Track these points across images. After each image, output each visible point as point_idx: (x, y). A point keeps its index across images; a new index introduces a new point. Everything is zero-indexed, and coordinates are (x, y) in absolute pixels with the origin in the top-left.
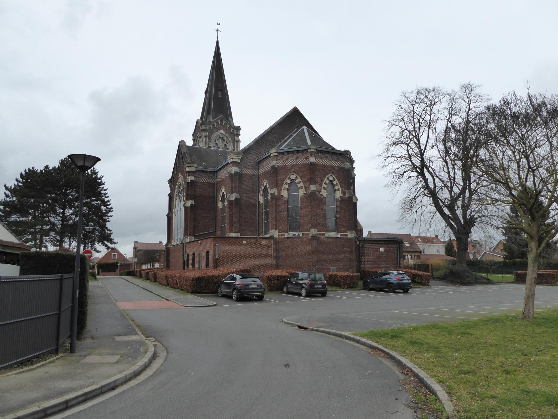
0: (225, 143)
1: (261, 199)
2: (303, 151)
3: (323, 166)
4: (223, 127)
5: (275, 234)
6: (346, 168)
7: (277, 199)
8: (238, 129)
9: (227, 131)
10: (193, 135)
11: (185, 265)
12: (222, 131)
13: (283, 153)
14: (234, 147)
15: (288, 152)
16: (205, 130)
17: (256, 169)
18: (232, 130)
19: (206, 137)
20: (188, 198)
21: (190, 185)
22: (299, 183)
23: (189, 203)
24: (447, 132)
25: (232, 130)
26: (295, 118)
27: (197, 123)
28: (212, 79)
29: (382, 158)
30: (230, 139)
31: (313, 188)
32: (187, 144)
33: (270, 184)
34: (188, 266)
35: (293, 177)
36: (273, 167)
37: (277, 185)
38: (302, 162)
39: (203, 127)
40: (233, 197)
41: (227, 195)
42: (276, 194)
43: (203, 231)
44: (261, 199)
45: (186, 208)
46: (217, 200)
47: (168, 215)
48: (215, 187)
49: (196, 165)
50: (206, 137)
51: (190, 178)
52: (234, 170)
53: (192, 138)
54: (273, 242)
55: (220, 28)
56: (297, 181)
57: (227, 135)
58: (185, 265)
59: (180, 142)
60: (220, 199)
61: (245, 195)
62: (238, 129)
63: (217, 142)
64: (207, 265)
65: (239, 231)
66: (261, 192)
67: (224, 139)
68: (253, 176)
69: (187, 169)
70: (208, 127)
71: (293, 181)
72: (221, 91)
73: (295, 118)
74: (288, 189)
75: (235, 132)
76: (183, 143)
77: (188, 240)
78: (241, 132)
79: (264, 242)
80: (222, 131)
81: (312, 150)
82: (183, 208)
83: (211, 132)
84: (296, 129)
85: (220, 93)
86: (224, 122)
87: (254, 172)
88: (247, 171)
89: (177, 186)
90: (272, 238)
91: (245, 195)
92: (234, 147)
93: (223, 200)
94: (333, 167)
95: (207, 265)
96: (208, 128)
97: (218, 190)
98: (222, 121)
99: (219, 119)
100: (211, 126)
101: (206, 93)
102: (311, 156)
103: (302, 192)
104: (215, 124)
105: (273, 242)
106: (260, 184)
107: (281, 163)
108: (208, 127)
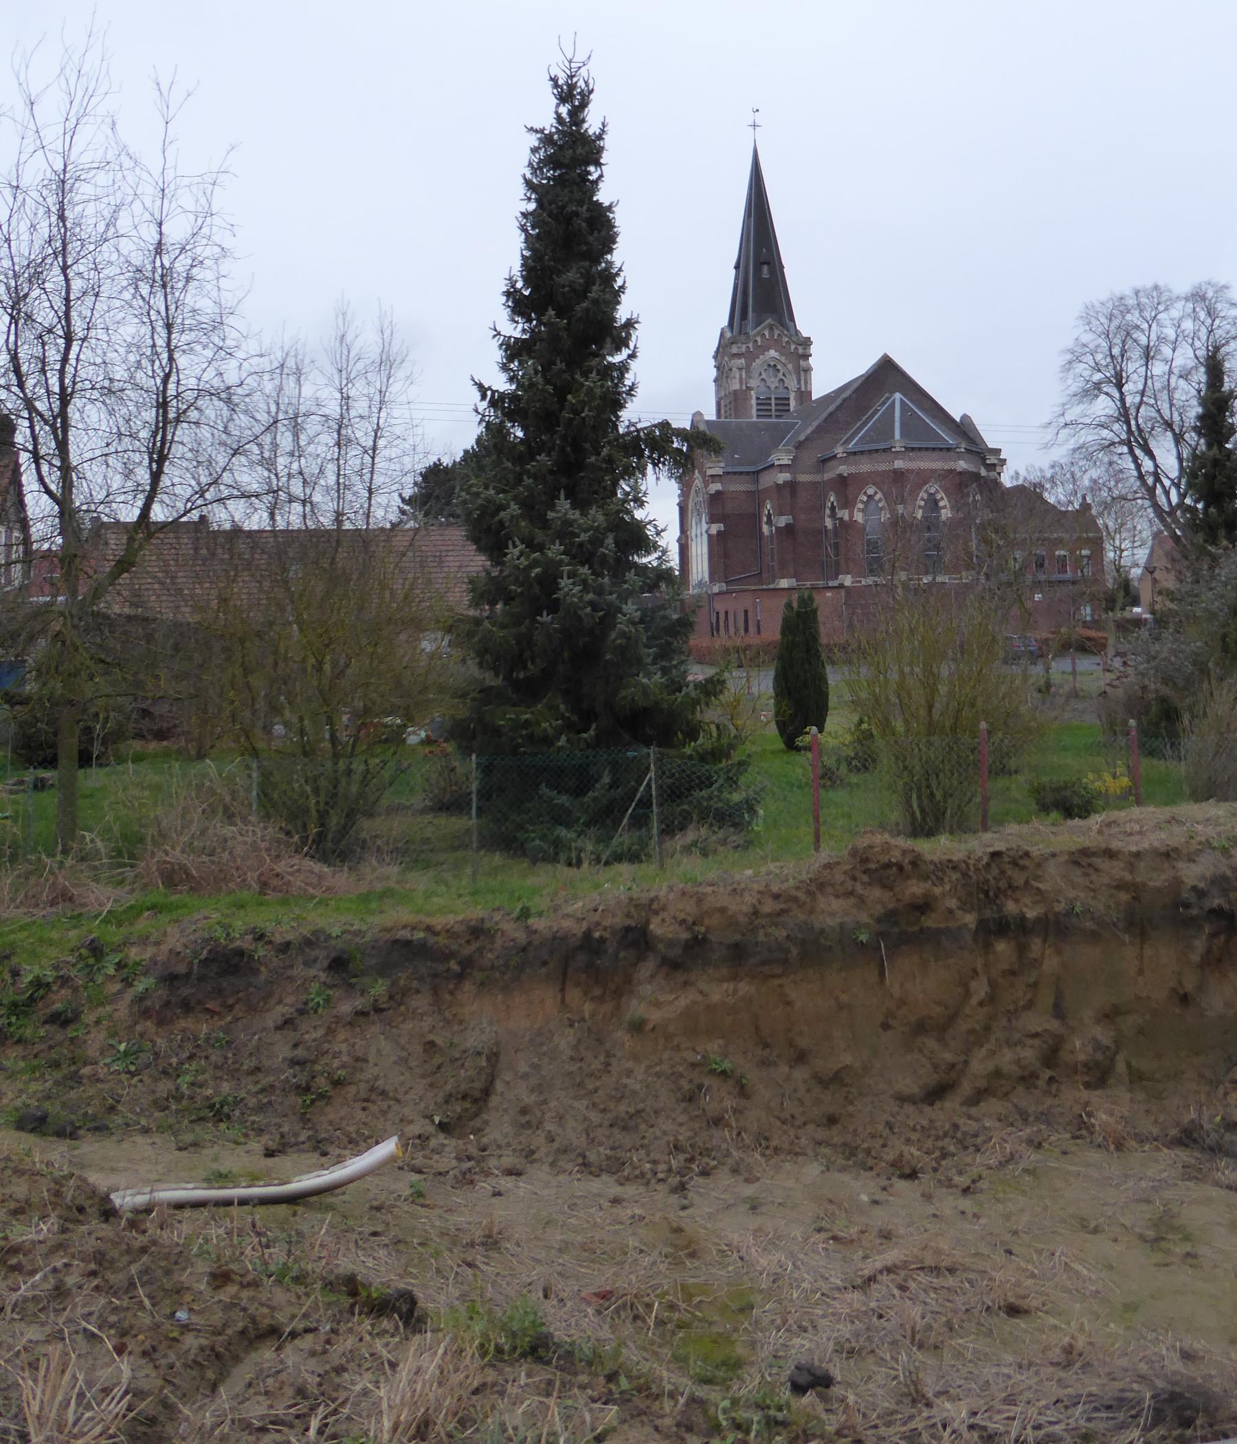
0: (780, 375)
1: (829, 523)
2: (884, 450)
3: (919, 472)
4: (776, 344)
5: (848, 580)
6: (959, 469)
7: (845, 527)
8: (807, 342)
9: (782, 349)
10: (715, 357)
11: (550, 1383)
12: (772, 353)
13: (855, 453)
14: (799, 383)
15: (862, 452)
16: (738, 356)
17: (819, 472)
18: (793, 347)
19: (740, 369)
20: (712, 520)
21: (716, 498)
22: (880, 500)
23: (715, 529)
24: (36, 1080)
25: (793, 347)
26: (886, 375)
27: (722, 335)
28: (748, 240)
29: (1052, 430)
30: (790, 366)
31: (900, 509)
32: (706, 418)
33: (838, 501)
34: (718, 631)
35: (870, 491)
36: (840, 476)
37: (848, 503)
38: (883, 467)
39: (734, 350)
40: (782, 521)
41: (774, 520)
42: (846, 518)
43: (740, 573)
44: (829, 523)
45: (710, 536)
46: (760, 522)
47: (679, 540)
48: (756, 497)
49: (723, 465)
50: (740, 369)
51: (715, 487)
52: (783, 477)
53: (713, 362)
54: (843, 592)
55: (759, 118)
56: (877, 497)
57: (783, 359)
58: (714, 630)
59: (694, 415)
60: (765, 519)
61: (803, 517)
62: (807, 342)
63: (764, 376)
64: (746, 630)
65: (795, 575)
66: (828, 512)
67: (779, 367)
68: (814, 484)
69: (709, 472)
70: (744, 346)
71: (870, 497)
72: (768, 263)
73: (886, 375)
74: (863, 511)
75: (801, 351)
76: (698, 418)
77: (716, 589)
78: (813, 349)
79: (829, 594)
80: (772, 353)
81: (898, 449)
82: (705, 537)
83: (750, 357)
84: (886, 395)
85: (765, 269)
86: (777, 332)
87: (817, 478)
88: (804, 478)
89: (693, 491)
90: (841, 586)
91: (803, 517)
92: (799, 383)
93: (769, 522)
94: (933, 471)
95: (746, 630)
96: (744, 349)
97: (761, 506)
98: (771, 328)
99: (764, 328)
100: (751, 345)
101: (737, 267)
102: (896, 459)
103: (885, 516)
104: (759, 339)
105: (843, 592)
106: (826, 497)
107: (853, 470)
108: (744, 346)
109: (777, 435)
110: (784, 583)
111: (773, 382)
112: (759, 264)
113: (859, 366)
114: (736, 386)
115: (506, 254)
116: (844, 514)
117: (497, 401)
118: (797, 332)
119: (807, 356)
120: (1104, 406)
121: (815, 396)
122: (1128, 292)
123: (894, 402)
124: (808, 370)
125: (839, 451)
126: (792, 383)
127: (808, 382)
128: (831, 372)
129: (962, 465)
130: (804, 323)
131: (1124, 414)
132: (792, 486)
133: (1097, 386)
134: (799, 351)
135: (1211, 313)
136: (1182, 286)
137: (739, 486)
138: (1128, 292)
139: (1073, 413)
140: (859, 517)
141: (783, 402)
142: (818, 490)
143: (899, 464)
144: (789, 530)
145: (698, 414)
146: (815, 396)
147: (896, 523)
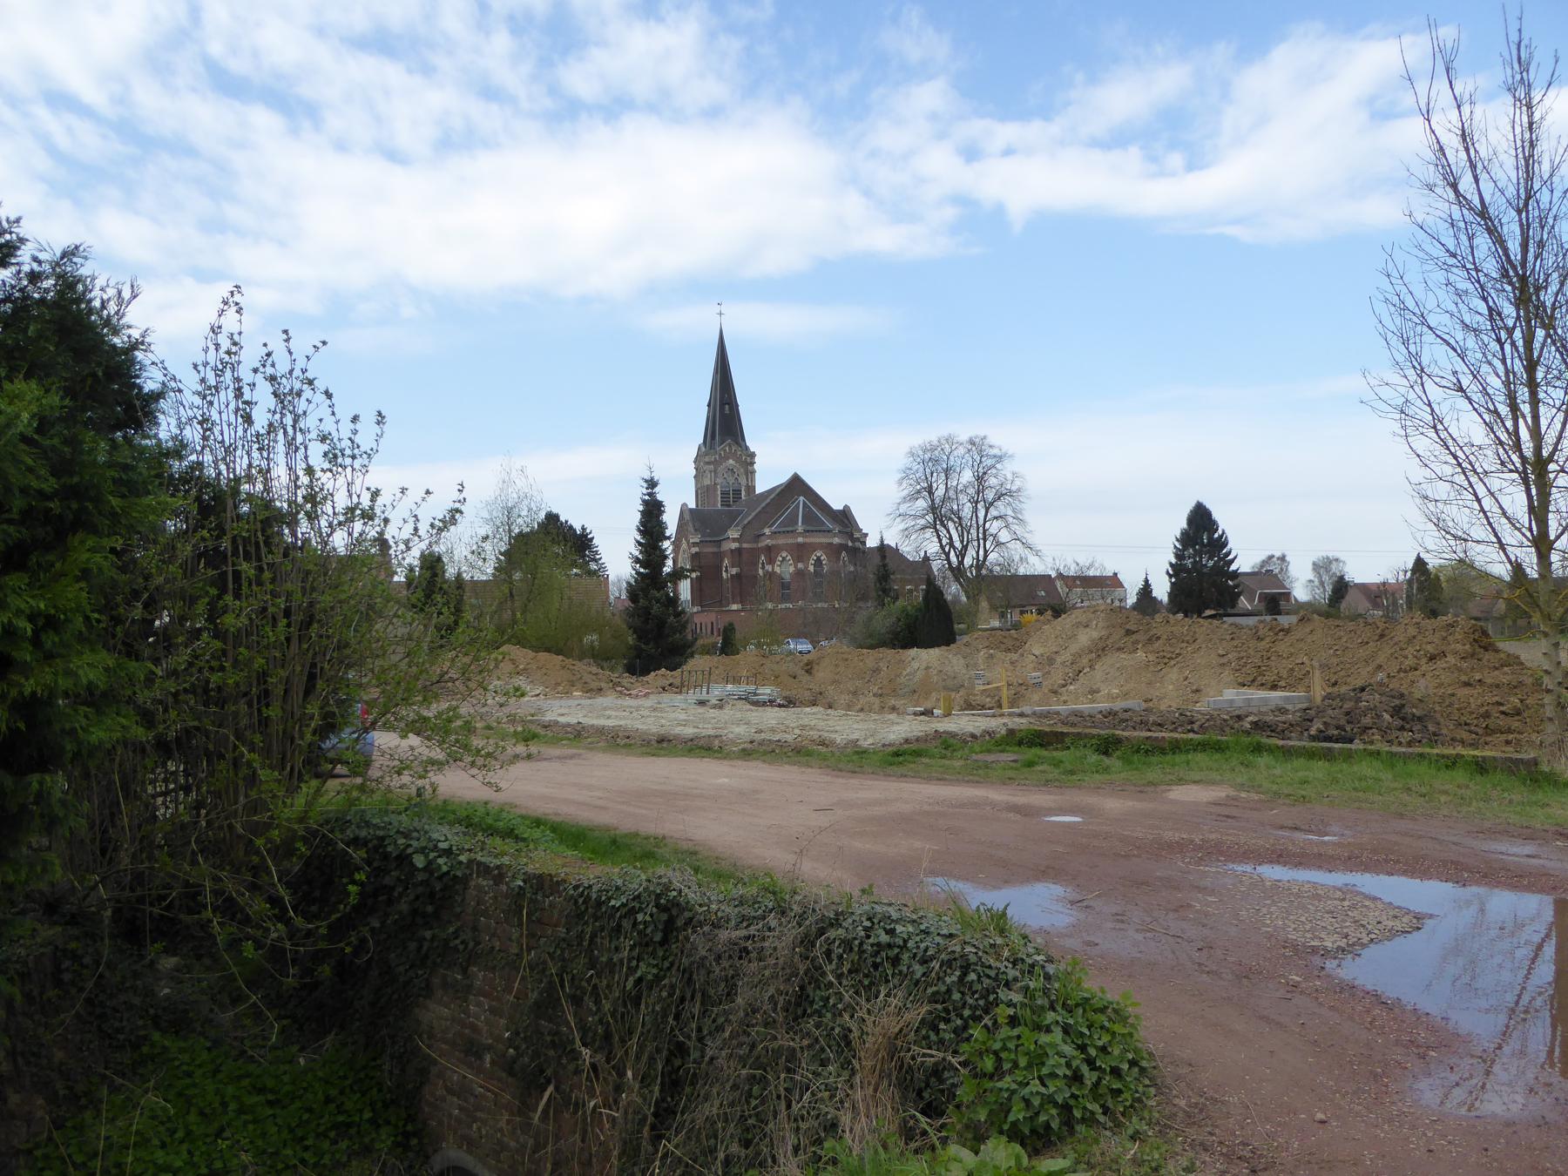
9: (738, 460)
26: (796, 485)
31: (800, 565)
37: (771, 561)
38: (791, 541)
40: (734, 571)
41: (729, 571)
48: (719, 556)
51: (696, 549)
52: (734, 545)
73: (796, 485)
83: (716, 463)
97: (722, 561)
103: (792, 569)
109: (732, 518)
110: (735, 607)
111: (731, 480)
112: (722, 405)
113: (783, 478)
114: (707, 482)
115: (636, 518)
116: (769, 568)
117: (637, 560)
118: (747, 448)
119: (752, 463)
120: (922, 504)
121: (758, 491)
122: (908, 461)
123: (797, 506)
124: (753, 472)
125: (767, 531)
126: (743, 481)
127: (753, 480)
128: (767, 477)
129: (836, 540)
130: (752, 443)
131: (933, 509)
132: (739, 550)
133: (919, 492)
134: (747, 460)
135: (980, 452)
136: (964, 437)
137: (710, 549)
138: (908, 461)
139: (903, 508)
140: (777, 570)
141: (737, 492)
142: (755, 553)
143: (800, 540)
144: (738, 576)
145: (684, 505)
146: (758, 491)
147: (800, 574)
